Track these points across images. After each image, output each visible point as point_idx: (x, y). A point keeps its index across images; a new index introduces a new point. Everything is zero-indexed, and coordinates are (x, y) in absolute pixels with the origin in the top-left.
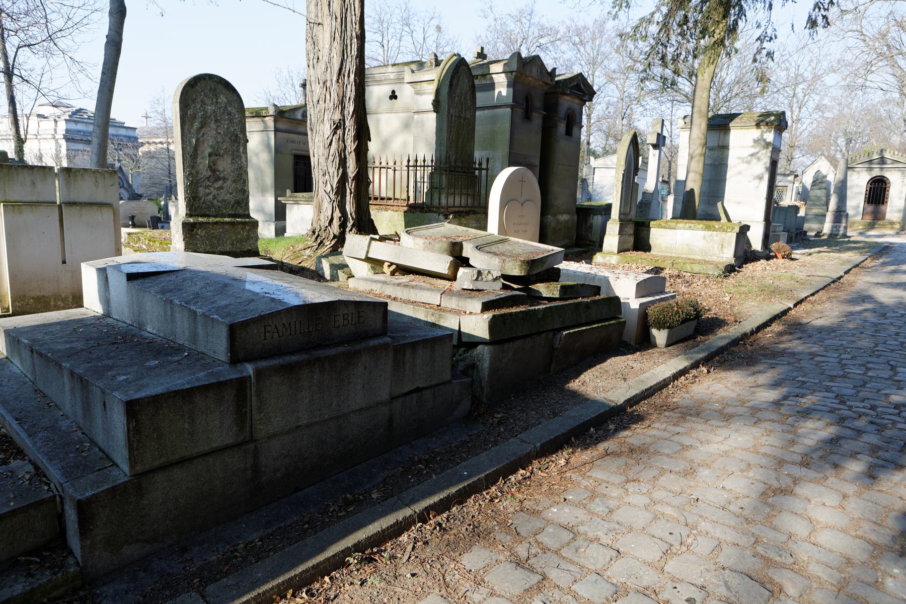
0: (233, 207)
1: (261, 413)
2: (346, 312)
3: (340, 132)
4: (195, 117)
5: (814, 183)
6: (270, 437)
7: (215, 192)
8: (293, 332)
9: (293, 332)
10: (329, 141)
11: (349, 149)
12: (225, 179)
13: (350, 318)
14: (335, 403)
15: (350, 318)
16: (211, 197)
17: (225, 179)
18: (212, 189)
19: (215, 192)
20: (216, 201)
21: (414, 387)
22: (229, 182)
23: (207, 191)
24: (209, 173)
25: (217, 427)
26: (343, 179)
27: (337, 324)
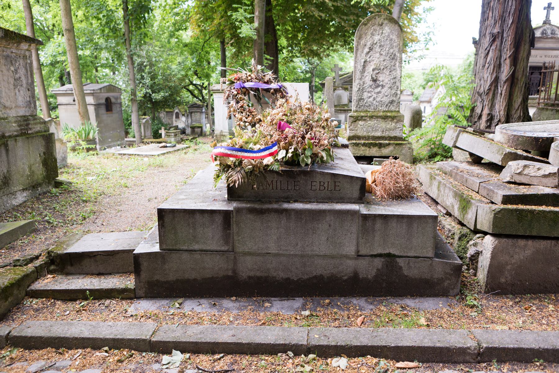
0: (387, 106)
1: (239, 236)
2: (322, 180)
3: (498, 42)
4: (365, 45)
5: (535, 69)
6: (245, 254)
7: (375, 96)
8: (275, 188)
9: (275, 188)
10: (487, 51)
11: (504, 56)
12: (383, 86)
13: (326, 185)
14: (300, 245)
15: (326, 185)
16: (371, 99)
17: (383, 86)
18: (373, 93)
19: (375, 96)
20: (375, 102)
21: (387, 251)
22: (386, 89)
23: (370, 95)
24: (371, 83)
25: (211, 238)
26: (496, 81)
27: (314, 188)
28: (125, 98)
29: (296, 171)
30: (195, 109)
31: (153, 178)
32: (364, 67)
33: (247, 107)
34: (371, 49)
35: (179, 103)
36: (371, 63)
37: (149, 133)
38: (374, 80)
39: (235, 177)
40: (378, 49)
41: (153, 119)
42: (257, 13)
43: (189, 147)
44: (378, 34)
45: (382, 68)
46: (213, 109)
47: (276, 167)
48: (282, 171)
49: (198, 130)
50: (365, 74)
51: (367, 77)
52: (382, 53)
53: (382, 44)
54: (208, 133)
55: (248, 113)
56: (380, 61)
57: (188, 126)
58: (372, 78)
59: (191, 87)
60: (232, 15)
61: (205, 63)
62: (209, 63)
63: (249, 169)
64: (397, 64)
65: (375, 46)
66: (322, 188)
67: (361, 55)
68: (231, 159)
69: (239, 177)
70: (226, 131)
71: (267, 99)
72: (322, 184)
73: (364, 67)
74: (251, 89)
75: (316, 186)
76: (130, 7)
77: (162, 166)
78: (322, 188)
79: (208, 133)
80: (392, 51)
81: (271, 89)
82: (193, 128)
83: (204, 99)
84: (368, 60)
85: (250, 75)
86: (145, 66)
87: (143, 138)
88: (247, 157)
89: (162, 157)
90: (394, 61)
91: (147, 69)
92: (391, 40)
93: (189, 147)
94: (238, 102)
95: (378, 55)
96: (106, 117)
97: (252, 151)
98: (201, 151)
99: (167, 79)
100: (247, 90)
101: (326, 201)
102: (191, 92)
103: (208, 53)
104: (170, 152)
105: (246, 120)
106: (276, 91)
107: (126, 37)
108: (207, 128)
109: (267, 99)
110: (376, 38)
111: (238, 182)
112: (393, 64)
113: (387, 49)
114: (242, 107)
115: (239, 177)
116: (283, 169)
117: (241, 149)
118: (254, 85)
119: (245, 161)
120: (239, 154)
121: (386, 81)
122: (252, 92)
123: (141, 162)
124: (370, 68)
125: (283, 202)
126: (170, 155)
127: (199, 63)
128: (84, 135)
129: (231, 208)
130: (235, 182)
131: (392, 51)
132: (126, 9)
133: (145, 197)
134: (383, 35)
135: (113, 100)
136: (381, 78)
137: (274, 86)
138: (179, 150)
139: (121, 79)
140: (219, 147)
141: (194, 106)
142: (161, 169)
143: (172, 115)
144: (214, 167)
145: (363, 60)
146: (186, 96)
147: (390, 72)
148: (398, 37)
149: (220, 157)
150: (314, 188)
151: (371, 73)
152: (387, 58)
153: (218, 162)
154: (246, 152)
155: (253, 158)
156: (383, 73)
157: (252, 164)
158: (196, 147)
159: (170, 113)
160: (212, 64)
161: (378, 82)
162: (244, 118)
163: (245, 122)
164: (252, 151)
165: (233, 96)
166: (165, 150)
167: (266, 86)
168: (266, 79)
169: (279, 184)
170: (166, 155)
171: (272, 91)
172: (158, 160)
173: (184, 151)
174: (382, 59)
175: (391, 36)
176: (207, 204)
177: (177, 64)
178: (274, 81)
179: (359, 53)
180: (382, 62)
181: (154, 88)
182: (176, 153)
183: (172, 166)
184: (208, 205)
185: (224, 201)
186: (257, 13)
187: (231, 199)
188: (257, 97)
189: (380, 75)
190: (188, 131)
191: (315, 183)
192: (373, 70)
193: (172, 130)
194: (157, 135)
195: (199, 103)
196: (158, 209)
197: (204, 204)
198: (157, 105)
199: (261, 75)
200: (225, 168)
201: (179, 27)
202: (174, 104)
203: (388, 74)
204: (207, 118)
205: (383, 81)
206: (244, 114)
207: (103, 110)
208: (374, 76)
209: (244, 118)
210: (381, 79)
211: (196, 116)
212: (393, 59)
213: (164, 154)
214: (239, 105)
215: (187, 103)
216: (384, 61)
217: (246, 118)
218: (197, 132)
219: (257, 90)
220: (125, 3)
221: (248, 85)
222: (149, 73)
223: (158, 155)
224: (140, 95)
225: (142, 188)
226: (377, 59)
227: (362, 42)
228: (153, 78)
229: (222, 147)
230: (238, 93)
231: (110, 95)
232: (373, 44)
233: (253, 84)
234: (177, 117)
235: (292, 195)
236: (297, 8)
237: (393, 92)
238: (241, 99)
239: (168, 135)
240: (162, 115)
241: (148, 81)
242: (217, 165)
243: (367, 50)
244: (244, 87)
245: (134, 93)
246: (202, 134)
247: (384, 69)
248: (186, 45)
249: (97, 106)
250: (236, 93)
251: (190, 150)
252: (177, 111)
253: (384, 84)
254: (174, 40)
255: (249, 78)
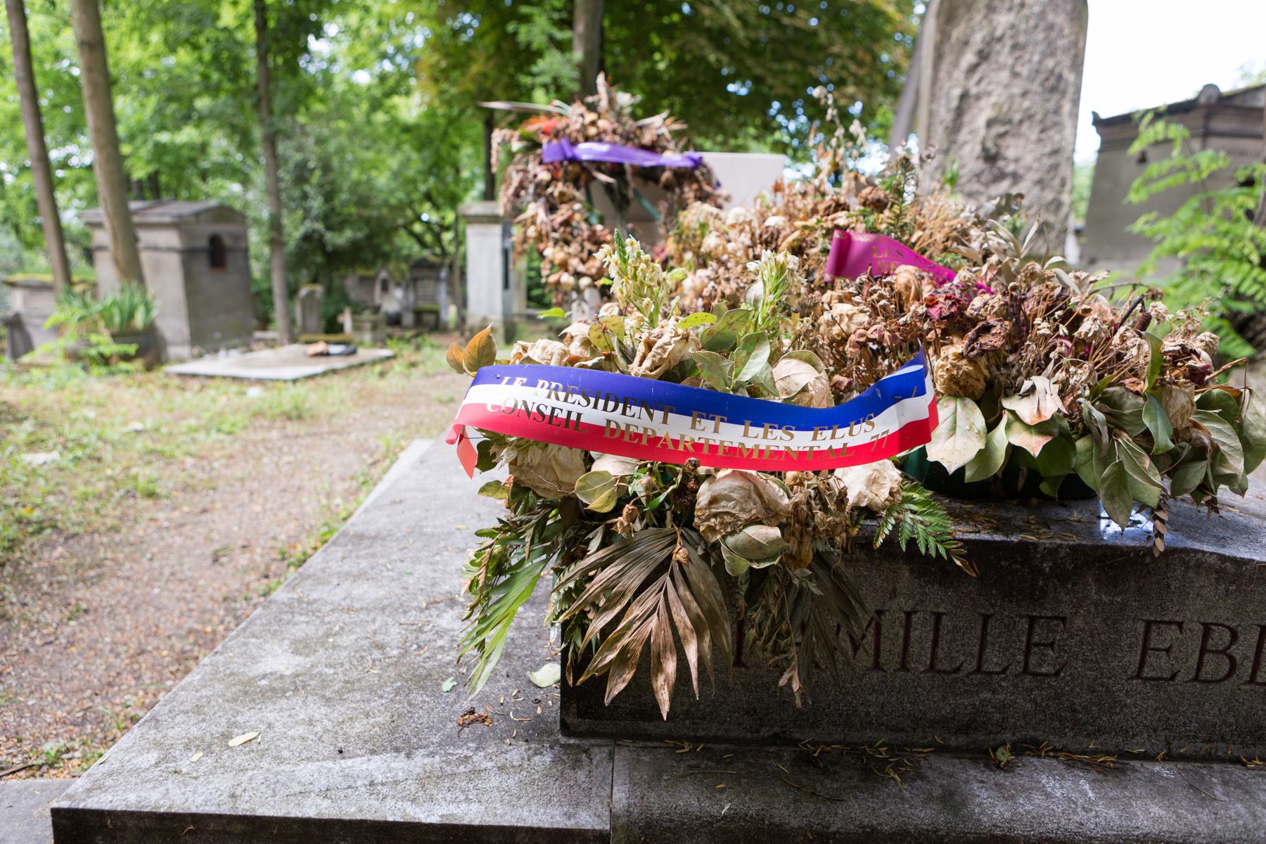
2: (1223, 613)
8: (890, 659)
9: (890, 659)
12: (1016, 177)
13: (1244, 649)
17: (1016, 177)
24: (980, 165)
27: (1158, 665)
28: (255, 238)
29: (1053, 552)
30: (424, 272)
31: (259, 459)
32: (960, 112)
33: (584, 226)
34: (983, 56)
35: (386, 257)
36: (984, 102)
37: (314, 321)
38: (990, 157)
39: (645, 622)
40: (1004, 55)
41: (329, 291)
42: (580, 27)
43: (394, 357)
44: (1010, 9)
45: (1017, 117)
46: (463, 274)
47: (926, 524)
48: (974, 550)
49: (429, 318)
50: (963, 136)
51: (967, 149)
52: (1018, 69)
53: (1022, 39)
54: (452, 325)
55: (588, 246)
56: (1011, 97)
57: (406, 309)
58: (985, 149)
59: (418, 228)
60: (515, 34)
61: (449, 171)
62: (457, 171)
63: (754, 550)
64: (1067, 107)
65: (998, 47)
66: (1215, 666)
67: (950, 75)
68: (609, 465)
69: (681, 617)
70: (496, 318)
71: (646, 204)
72: (1220, 638)
73: (960, 112)
74: (598, 165)
75: (1178, 649)
76: (272, 24)
77: (300, 417)
78: (1215, 666)
79: (452, 325)
80: (1050, 63)
81: (662, 168)
82: (418, 314)
83: (444, 253)
84: (974, 91)
85: (593, 123)
86: (312, 171)
87: (296, 331)
88: (734, 457)
89: (301, 389)
90: (1056, 97)
91: (316, 177)
92: (1051, 27)
93: (394, 357)
94: (552, 209)
95: (1004, 76)
96: (209, 280)
97: (751, 407)
98: (429, 367)
99: (363, 202)
100: (584, 169)
101: (1233, 750)
102: (419, 239)
103: (456, 147)
104: (335, 371)
105: (581, 268)
106: (683, 176)
107: (262, 91)
108: (450, 314)
109: (646, 204)
110: (1003, 20)
111: (670, 666)
112: (1051, 105)
113: (1036, 58)
114: (567, 223)
115: (681, 617)
116: (964, 532)
117: (676, 388)
118: (608, 153)
119: (720, 485)
120: (679, 428)
121: (1028, 159)
122: (603, 178)
123: (236, 401)
124: (980, 116)
125: (941, 750)
126: (335, 380)
127: (435, 168)
128: (117, 319)
129: (588, 819)
130: (647, 662)
131: (1050, 63)
132: (261, 26)
133: (209, 539)
134: (1026, 11)
135: (228, 242)
136: (1012, 149)
137: (673, 158)
138: (362, 365)
139: (249, 196)
140: (511, 372)
141: (421, 265)
142: (292, 428)
143: (373, 285)
144: (472, 505)
145: (957, 92)
146: (404, 242)
147: (1043, 131)
148: (1072, 20)
149: (522, 448)
150: (1158, 665)
151: (982, 132)
152: (1035, 87)
153: (502, 472)
154: (735, 419)
155: (776, 463)
156: (1018, 135)
157: (770, 513)
158: (416, 357)
159: (367, 281)
160: (465, 174)
161: (1001, 164)
162: (574, 262)
163: (578, 275)
164: (751, 407)
165: (538, 186)
166: (320, 366)
167: (649, 160)
168: (647, 138)
169: (921, 632)
170: (319, 380)
171: (666, 175)
172: (289, 397)
173: (378, 368)
174: (1016, 90)
175: (1050, 17)
176: (420, 761)
177: (385, 172)
178: (671, 145)
179: (945, 66)
180: (1018, 100)
181: (332, 219)
182: (354, 374)
183: (332, 416)
184: (424, 780)
185: (534, 733)
186: (580, 27)
187: (585, 724)
188: (618, 196)
189: (1008, 141)
190: (408, 319)
191: (1171, 634)
192: (990, 124)
193: (367, 315)
194: (333, 327)
195: (433, 259)
196: (56, 812)
197: (399, 765)
198: (337, 259)
199: (630, 124)
200: (554, 522)
201: (392, 87)
202: (376, 257)
203: (1034, 137)
204: (451, 293)
205: (1017, 161)
206: (574, 248)
207: (202, 264)
208: (990, 144)
209: (574, 262)
210: (1011, 153)
211: (426, 286)
212: (1053, 89)
213: (311, 377)
214: (559, 218)
215: (407, 258)
216: (1024, 94)
217: (583, 262)
218: (426, 323)
219: (616, 170)
220: (260, 7)
221: (586, 151)
222: (321, 186)
223: (295, 381)
224: (295, 231)
225: (205, 502)
226: (999, 90)
227: (957, 33)
228: (329, 197)
229: (532, 372)
230: (554, 179)
231: (221, 229)
232: (992, 40)
233: (604, 148)
234: (385, 287)
235: (1003, 707)
236: (659, 49)
237: (1049, 196)
238: (564, 199)
239: (357, 327)
240: (351, 283)
241: (316, 204)
242: (492, 488)
243: (969, 58)
244: (574, 160)
245: (275, 225)
246: (437, 327)
247: (1021, 122)
248: (407, 129)
249: (188, 255)
250: (544, 176)
251: (398, 366)
252: (383, 275)
253: (1021, 171)
254: (380, 117)
255: (592, 131)
